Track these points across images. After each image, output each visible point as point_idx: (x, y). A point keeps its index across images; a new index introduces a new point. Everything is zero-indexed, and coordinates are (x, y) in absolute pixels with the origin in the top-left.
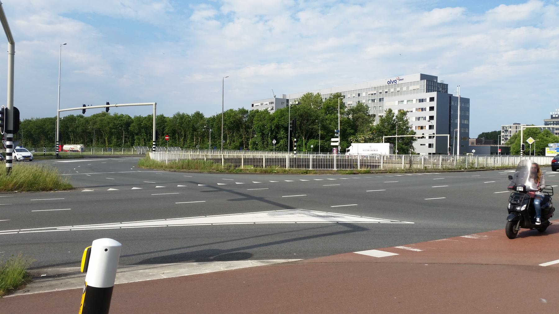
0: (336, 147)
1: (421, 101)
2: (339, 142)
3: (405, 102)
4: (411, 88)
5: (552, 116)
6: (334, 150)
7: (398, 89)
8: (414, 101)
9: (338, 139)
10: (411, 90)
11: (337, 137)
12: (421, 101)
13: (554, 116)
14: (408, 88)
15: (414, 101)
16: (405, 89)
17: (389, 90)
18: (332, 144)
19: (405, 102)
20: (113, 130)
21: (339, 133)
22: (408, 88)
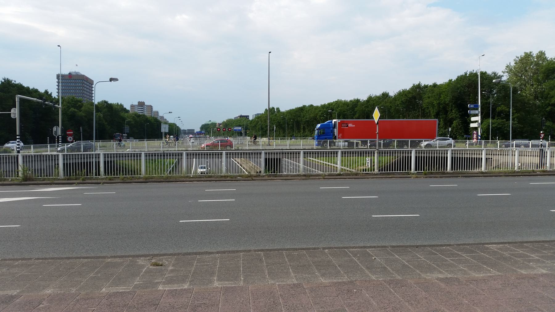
0: (476, 129)
2: (480, 122)
6: (474, 134)
9: (478, 118)
11: (476, 115)
18: (472, 125)
20: (321, 118)
21: (480, 109)
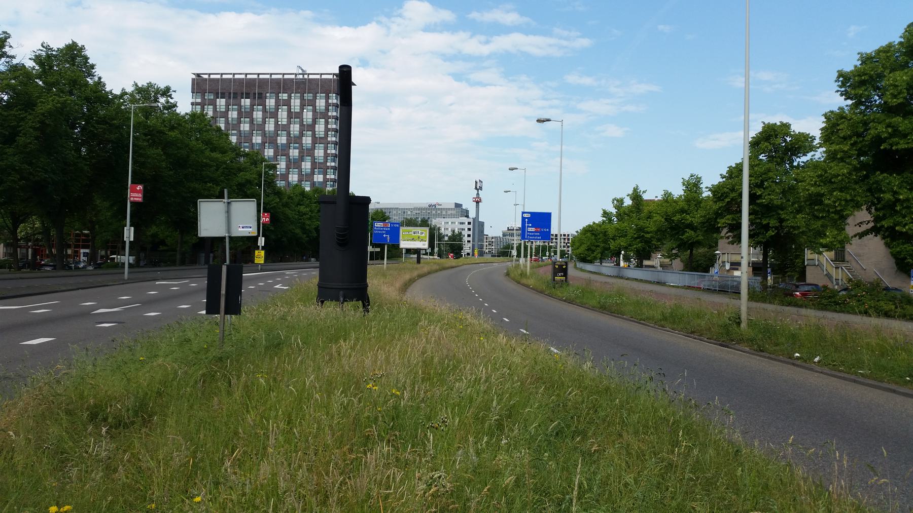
1: (462, 223)
3: (450, 223)
4: (449, 212)
5: (508, 228)
7: (439, 212)
8: (457, 223)
10: (449, 215)
12: (462, 223)
13: (510, 228)
14: (446, 212)
15: (457, 223)
16: (444, 213)
17: (431, 212)
19: (450, 223)
22: (446, 212)
